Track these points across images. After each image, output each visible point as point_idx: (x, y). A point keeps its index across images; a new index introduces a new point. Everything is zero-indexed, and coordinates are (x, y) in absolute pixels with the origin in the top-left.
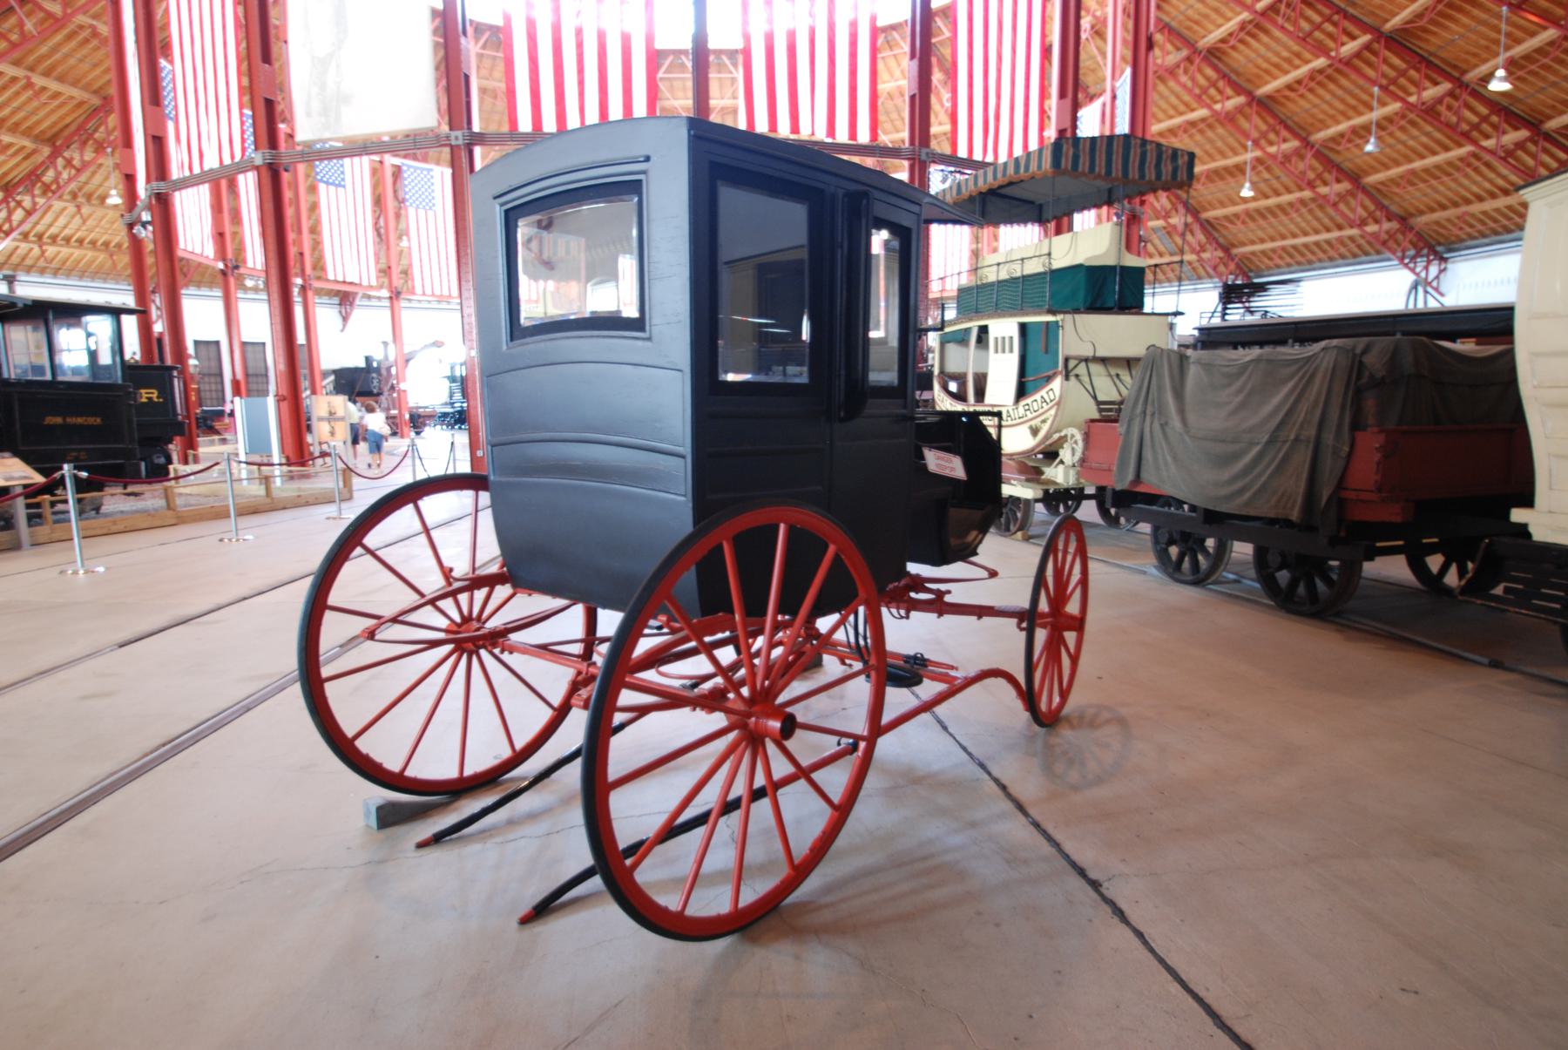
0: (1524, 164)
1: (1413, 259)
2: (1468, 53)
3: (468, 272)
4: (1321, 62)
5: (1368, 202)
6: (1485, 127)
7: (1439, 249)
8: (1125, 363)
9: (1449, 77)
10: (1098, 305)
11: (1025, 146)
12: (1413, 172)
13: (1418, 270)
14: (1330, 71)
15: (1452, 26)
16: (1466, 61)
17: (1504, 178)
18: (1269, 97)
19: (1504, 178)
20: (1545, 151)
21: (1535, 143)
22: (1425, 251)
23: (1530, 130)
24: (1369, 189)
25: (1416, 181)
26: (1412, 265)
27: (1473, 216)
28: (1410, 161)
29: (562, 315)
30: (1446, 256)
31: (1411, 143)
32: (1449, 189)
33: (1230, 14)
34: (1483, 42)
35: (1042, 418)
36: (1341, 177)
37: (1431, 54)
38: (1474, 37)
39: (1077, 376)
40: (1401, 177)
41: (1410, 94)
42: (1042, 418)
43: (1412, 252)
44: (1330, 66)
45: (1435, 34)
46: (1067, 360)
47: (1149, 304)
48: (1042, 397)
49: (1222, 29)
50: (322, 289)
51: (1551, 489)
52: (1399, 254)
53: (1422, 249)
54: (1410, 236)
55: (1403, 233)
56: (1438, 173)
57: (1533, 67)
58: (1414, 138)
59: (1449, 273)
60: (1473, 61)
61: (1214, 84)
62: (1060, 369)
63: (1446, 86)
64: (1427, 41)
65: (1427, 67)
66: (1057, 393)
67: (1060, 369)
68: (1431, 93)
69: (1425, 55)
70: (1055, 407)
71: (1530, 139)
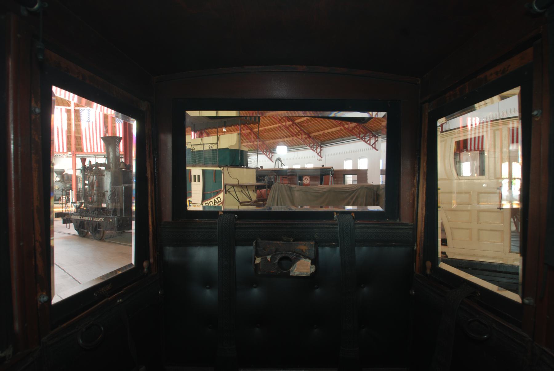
1: (266, 152)
3: (267, 207)
5: (254, 136)
8: (246, 187)
10: (234, 164)
12: (265, 129)
13: (267, 155)
17: (286, 133)
19: (286, 133)
20: (295, 128)
21: (293, 126)
24: (255, 133)
25: (266, 132)
26: (266, 154)
27: (326, 133)
28: (265, 127)
29: (111, 273)
30: (273, 152)
31: (265, 122)
32: (274, 135)
36: (248, 129)
39: (229, 192)
40: (263, 130)
43: (265, 150)
46: (225, 186)
47: (381, 176)
48: (214, 200)
50: (71, 144)
51: (452, 240)
52: (263, 151)
53: (268, 150)
54: (265, 146)
55: (263, 145)
56: (274, 130)
58: (265, 120)
59: (274, 156)
62: (223, 189)
66: (222, 199)
67: (223, 189)
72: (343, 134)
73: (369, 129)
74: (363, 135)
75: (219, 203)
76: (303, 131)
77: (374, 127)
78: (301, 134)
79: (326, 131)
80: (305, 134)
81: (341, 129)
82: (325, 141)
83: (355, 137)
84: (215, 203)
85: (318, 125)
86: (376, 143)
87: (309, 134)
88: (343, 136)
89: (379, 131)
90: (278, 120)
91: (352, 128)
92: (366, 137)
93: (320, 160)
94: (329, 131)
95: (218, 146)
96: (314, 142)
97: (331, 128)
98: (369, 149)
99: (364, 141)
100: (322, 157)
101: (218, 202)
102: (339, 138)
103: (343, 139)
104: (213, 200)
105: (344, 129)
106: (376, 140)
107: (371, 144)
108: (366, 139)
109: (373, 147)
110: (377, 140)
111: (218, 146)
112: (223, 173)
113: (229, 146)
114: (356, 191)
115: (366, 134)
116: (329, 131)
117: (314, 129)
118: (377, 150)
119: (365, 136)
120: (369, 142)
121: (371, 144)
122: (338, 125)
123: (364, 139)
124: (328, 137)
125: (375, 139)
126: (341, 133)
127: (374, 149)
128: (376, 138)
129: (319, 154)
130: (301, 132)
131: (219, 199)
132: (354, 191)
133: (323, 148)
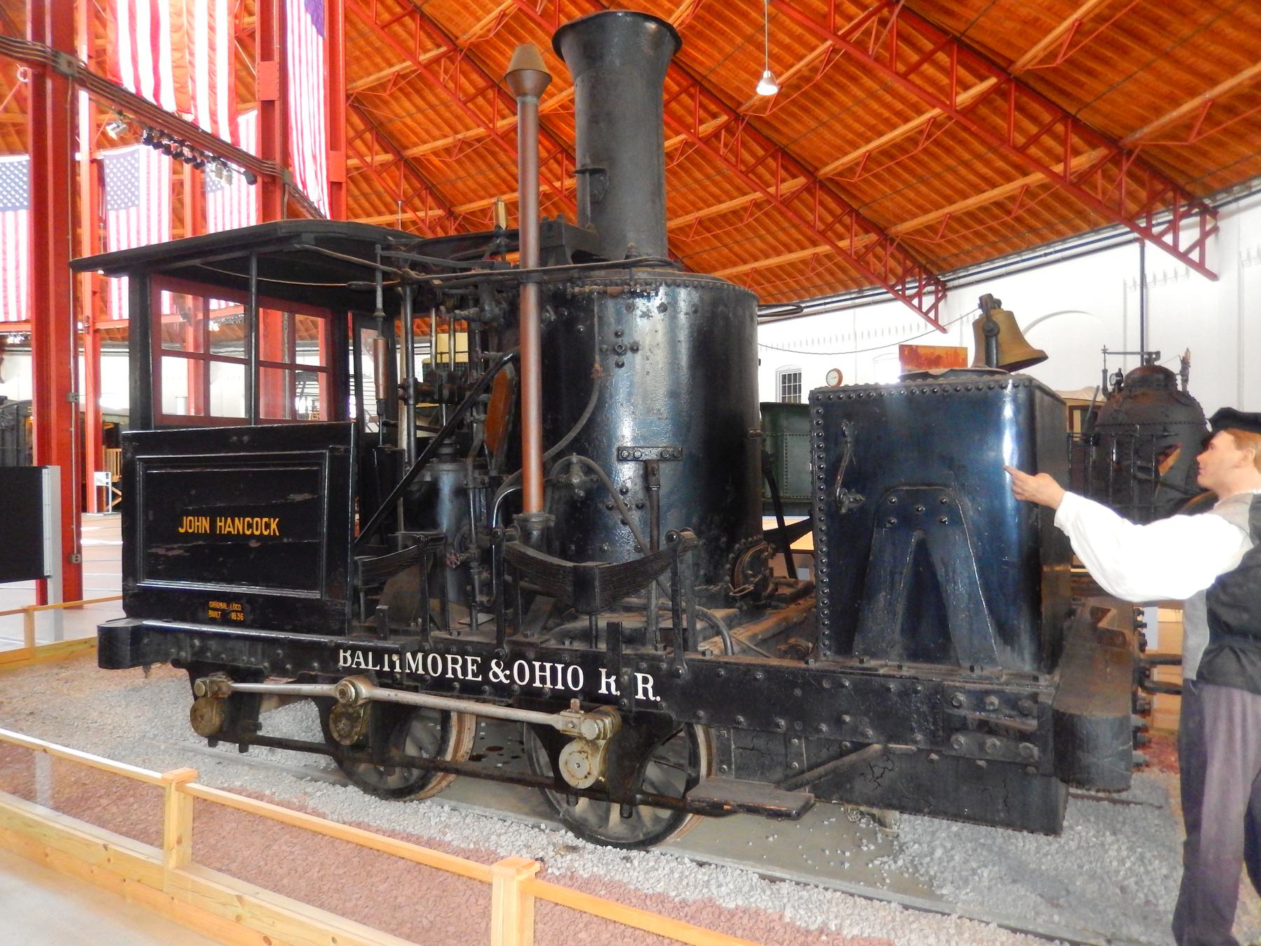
6: (838, 227)
11: (128, 213)
15: (828, 103)
18: (416, 159)
33: (394, 60)
41: (769, 186)
49: (372, 78)
57: (903, 158)
61: (838, 219)
63: (801, 180)
78: (848, 228)
86: (1210, 241)
90: (743, 168)
92: (907, 286)
98: (1170, 274)
106: (1208, 227)
107: (924, 309)
109: (929, 320)
118: (1213, 276)
120: (1168, 239)
124: (980, 228)
125: (1203, 224)
127: (1194, 274)
129: (1195, 255)
130: (1059, 128)
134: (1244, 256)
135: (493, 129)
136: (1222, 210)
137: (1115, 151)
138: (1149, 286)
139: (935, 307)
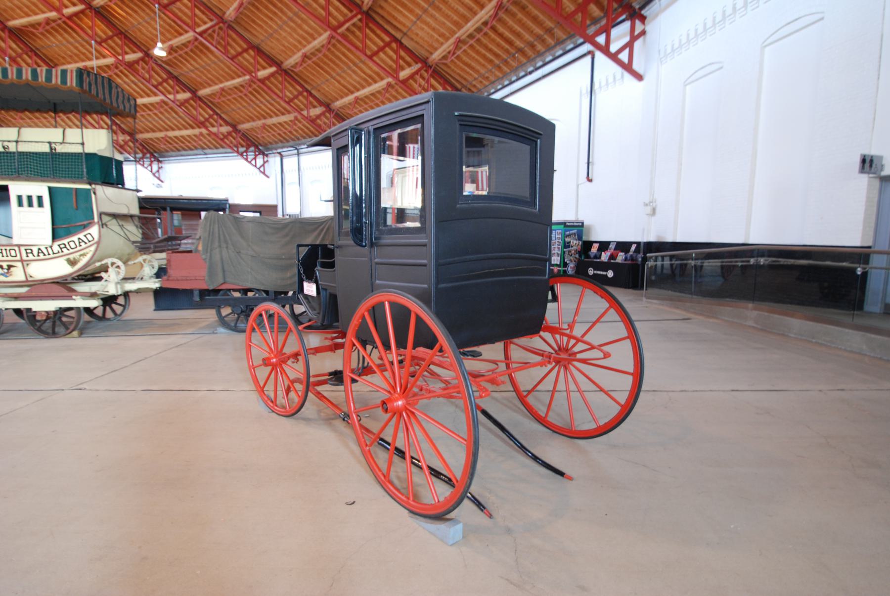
0: (192, 113)
2: (59, 55)
4: (53, 14)
7: (156, 155)
9: (141, 50)
10: (106, 181)
14: (60, 22)
16: (59, 60)
20: (200, 106)
22: (148, 155)
23: (191, 93)
27: (170, 138)
30: (161, 159)
34: (70, 53)
35: (82, 252)
37: (37, 49)
38: (64, 49)
42: (82, 252)
43: (140, 155)
44: (60, 19)
45: (40, 38)
46: (101, 214)
48: (79, 239)
53: (146, 154)
60: (63, 61)
63: (139, 55)
64: (34, 40)
65: (125, 38)
68: (131, 57)
69: (34, 49)
70: (95, 246)
71: (191, 98)
72: (205, 143)
73: (253, 140)
74: (244, 149)
75: (89, 244)
76: (120, 127)
77: (261, 138)
79: (171, 134)
80: (123, 134)
81: (201, 134)
82: (167, 151)
83: (230, 150)
84: (80, 243)
85: (154, 120)
86: (637, 44)
87: (133, 134)
88: (206, 147)
89: (270, 146)
91: (223, 134)
93: (159, 186)
94: (177, 133)
95: (83, 147)
96: (145, 151)
97: (180, 129)
99: (247, 159)
100: (162, 181)
101: (87, 241)
102: (196, 148)
103: (204, 151)
104: (75, 238)
105: (208, 134)
106: (266, 159)
108: (249, 157)
109: (261, 172)
110: (267, 161)
111: (83, 147)
112: (95, 193)
113: (98, 151)
114: (324, 224)
115: (247, 149)
116: (177, 133)
117: (143, 125)
119: (246, 152)
120: (253, 162)
121: (258, 166)
122: (194, 125)
123: (245, 157)
126: (201, 140)
127: (262, 175)
128: (265, 157)
129: (624, 56)
131: (89, 236)
132: (323, 222)
133: (164, 164)
134: (662, 54)
135: (256, 77)
136: (269, 155)
137: (328, 109)
138: (596, 91)
139: (630, 45)
